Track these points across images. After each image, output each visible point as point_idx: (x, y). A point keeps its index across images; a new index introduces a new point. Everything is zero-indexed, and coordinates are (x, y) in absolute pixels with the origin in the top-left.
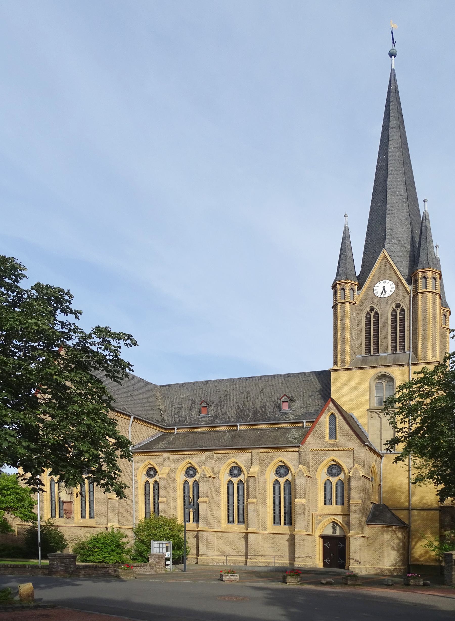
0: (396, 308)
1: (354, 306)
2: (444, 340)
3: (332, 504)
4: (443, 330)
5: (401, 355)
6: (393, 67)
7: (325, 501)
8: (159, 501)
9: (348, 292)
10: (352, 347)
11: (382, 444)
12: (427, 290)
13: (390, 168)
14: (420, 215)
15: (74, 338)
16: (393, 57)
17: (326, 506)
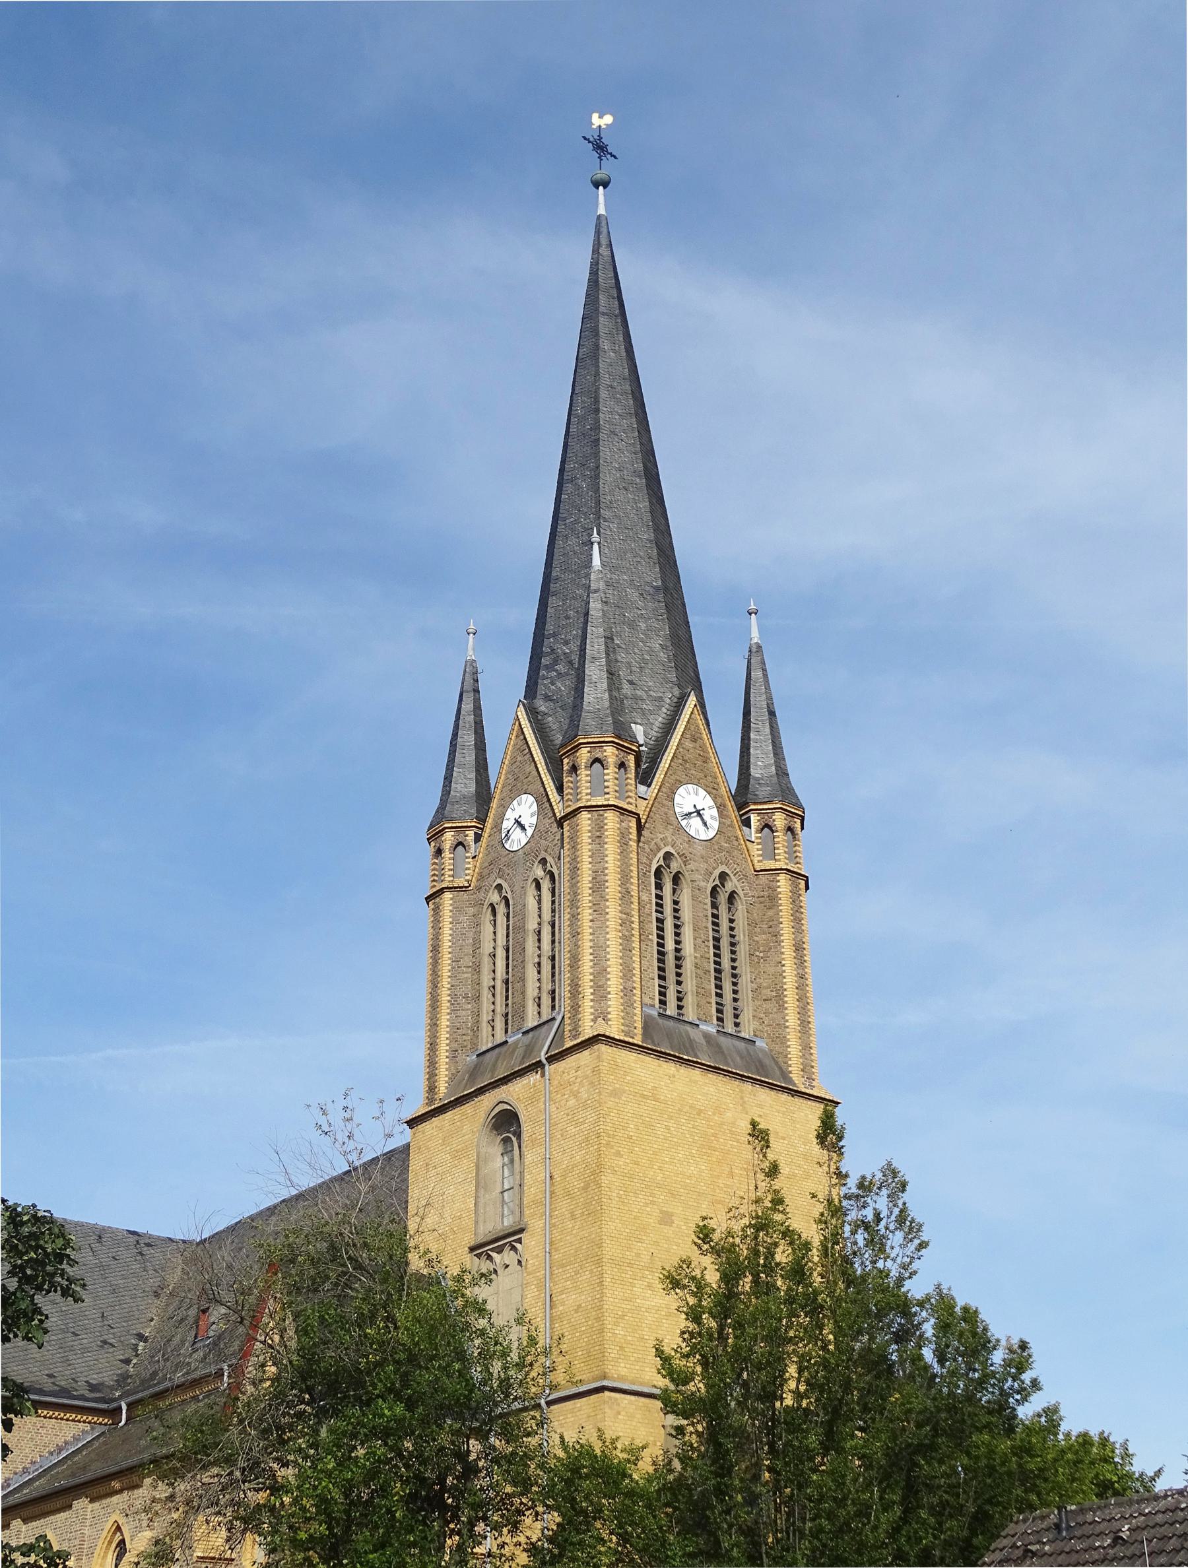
2: (770, 913)
4: (763, 879)
6: (602, 210)
16: (601, 188)
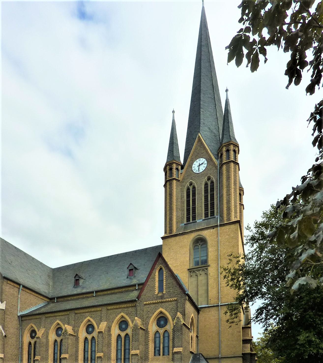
0: (207, 180)
1: (179, 183)
3: (160, 355)
5: (211, 220)
7: (155, 352)
8: (35, 359)
9: (174, 171)
10: (177, 217)
11: (78, 291)
12: (230, 160)
13: (202, 74)
14: (223, 111)
15: (275, 321)
17: (156, 357)
